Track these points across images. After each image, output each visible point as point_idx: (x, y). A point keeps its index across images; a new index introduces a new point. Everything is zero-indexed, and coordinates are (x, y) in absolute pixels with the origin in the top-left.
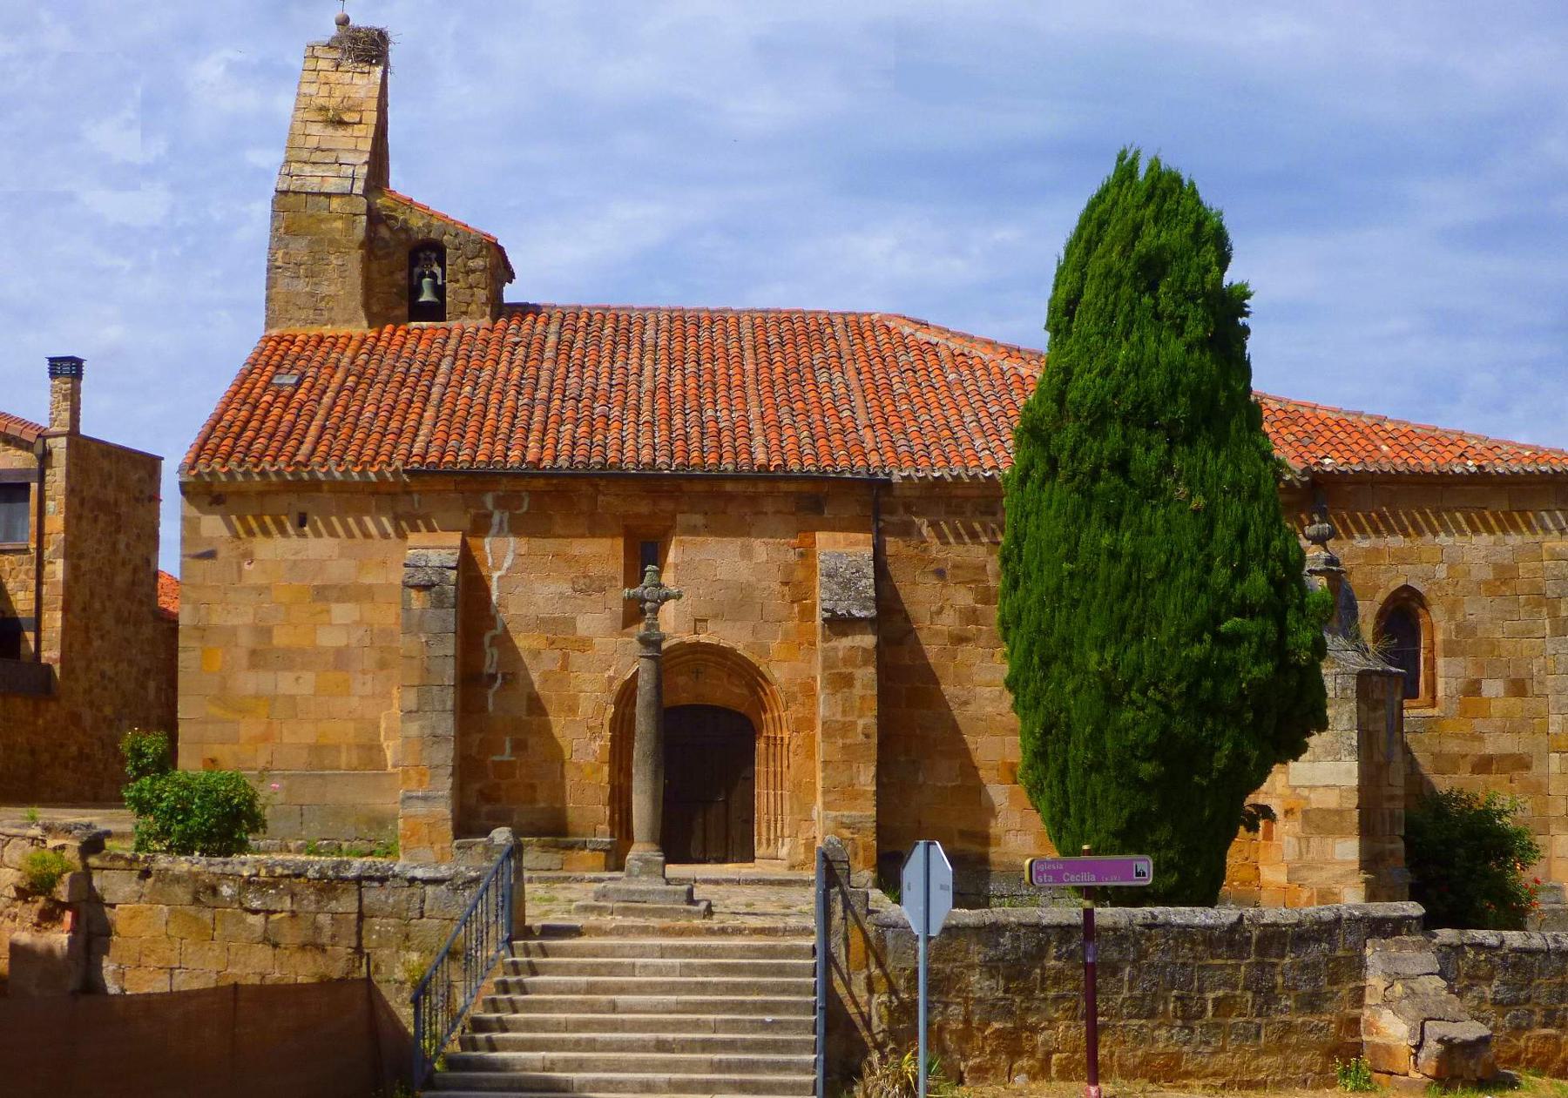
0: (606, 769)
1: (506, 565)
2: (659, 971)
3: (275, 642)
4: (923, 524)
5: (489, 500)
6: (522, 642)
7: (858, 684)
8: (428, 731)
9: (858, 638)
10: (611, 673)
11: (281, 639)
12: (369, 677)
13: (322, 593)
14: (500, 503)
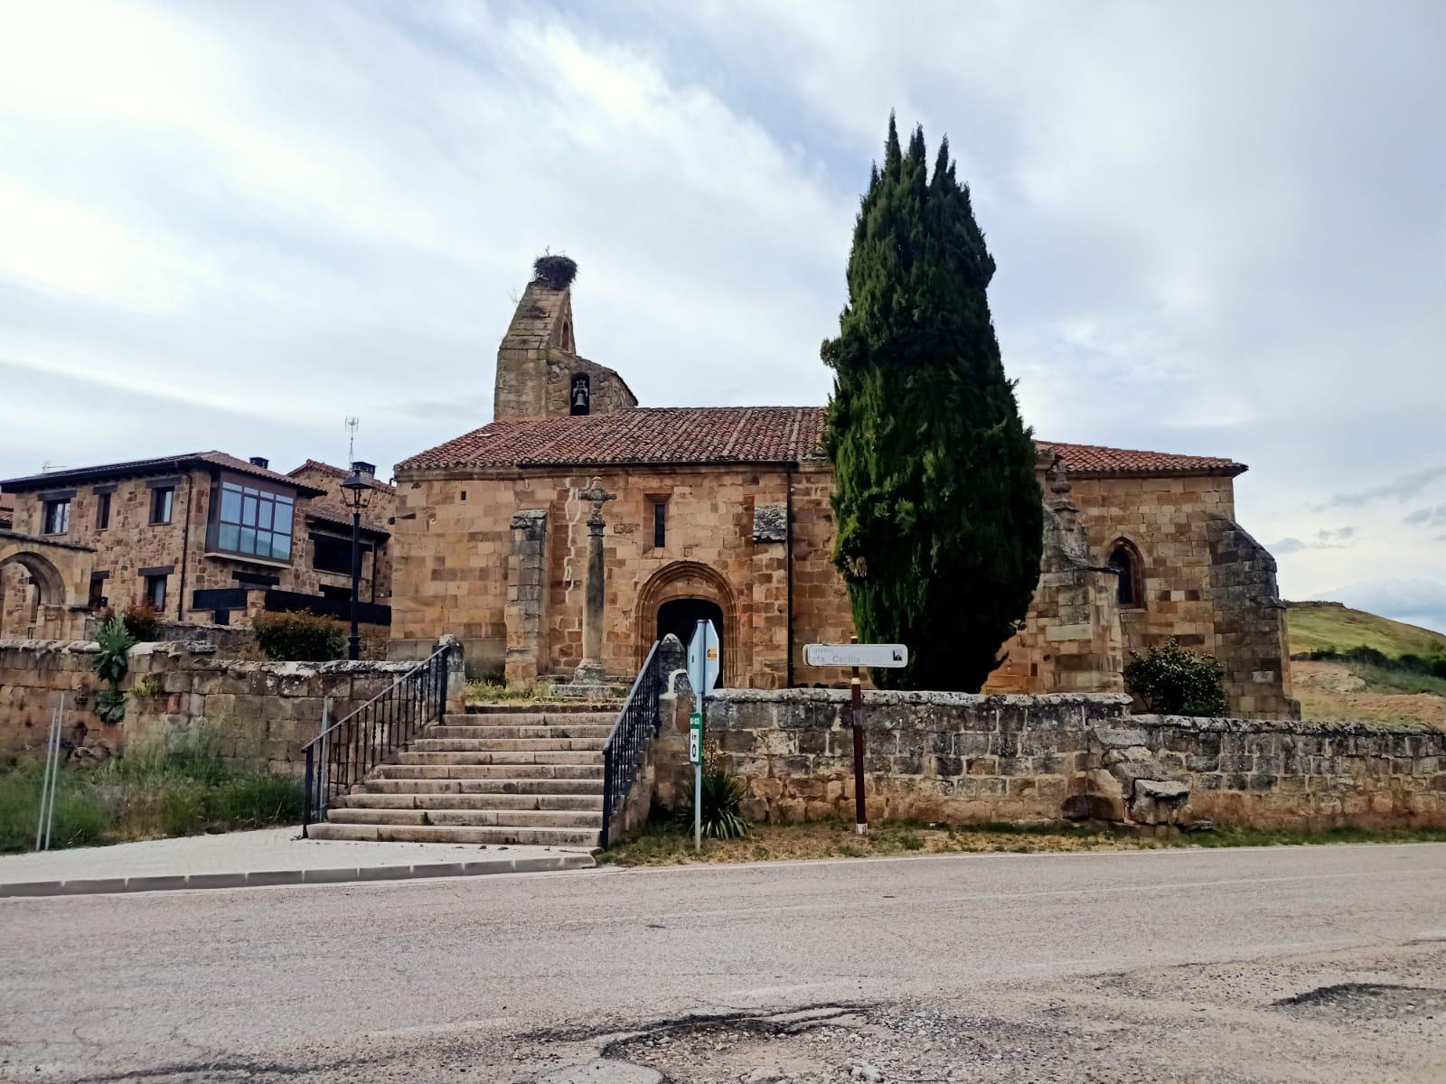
7: (774, 580)
8: (522, 612)
11: (449, 564)
13: (473, 537)
14: (573, 484)
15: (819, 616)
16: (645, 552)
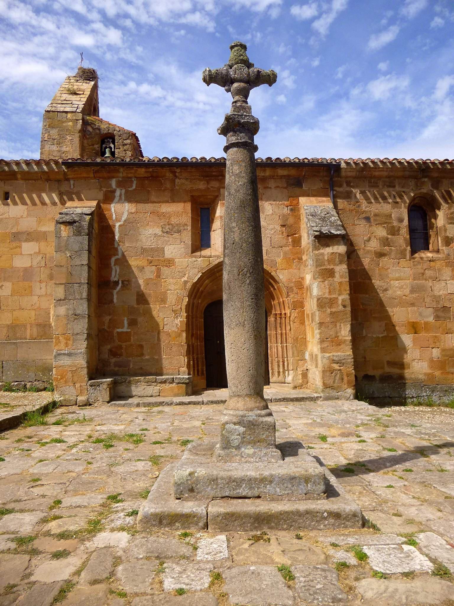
0: (184, 335)
1: (123, 219)
4: (357, 192)
5: (113, 183)
6: (133, 262)
7: (337, 275)
8: (71, 312)
12: (43, 285)
13: (17, 237)
14: (120, 184)
15: (365, 310)
16: (193, 252)
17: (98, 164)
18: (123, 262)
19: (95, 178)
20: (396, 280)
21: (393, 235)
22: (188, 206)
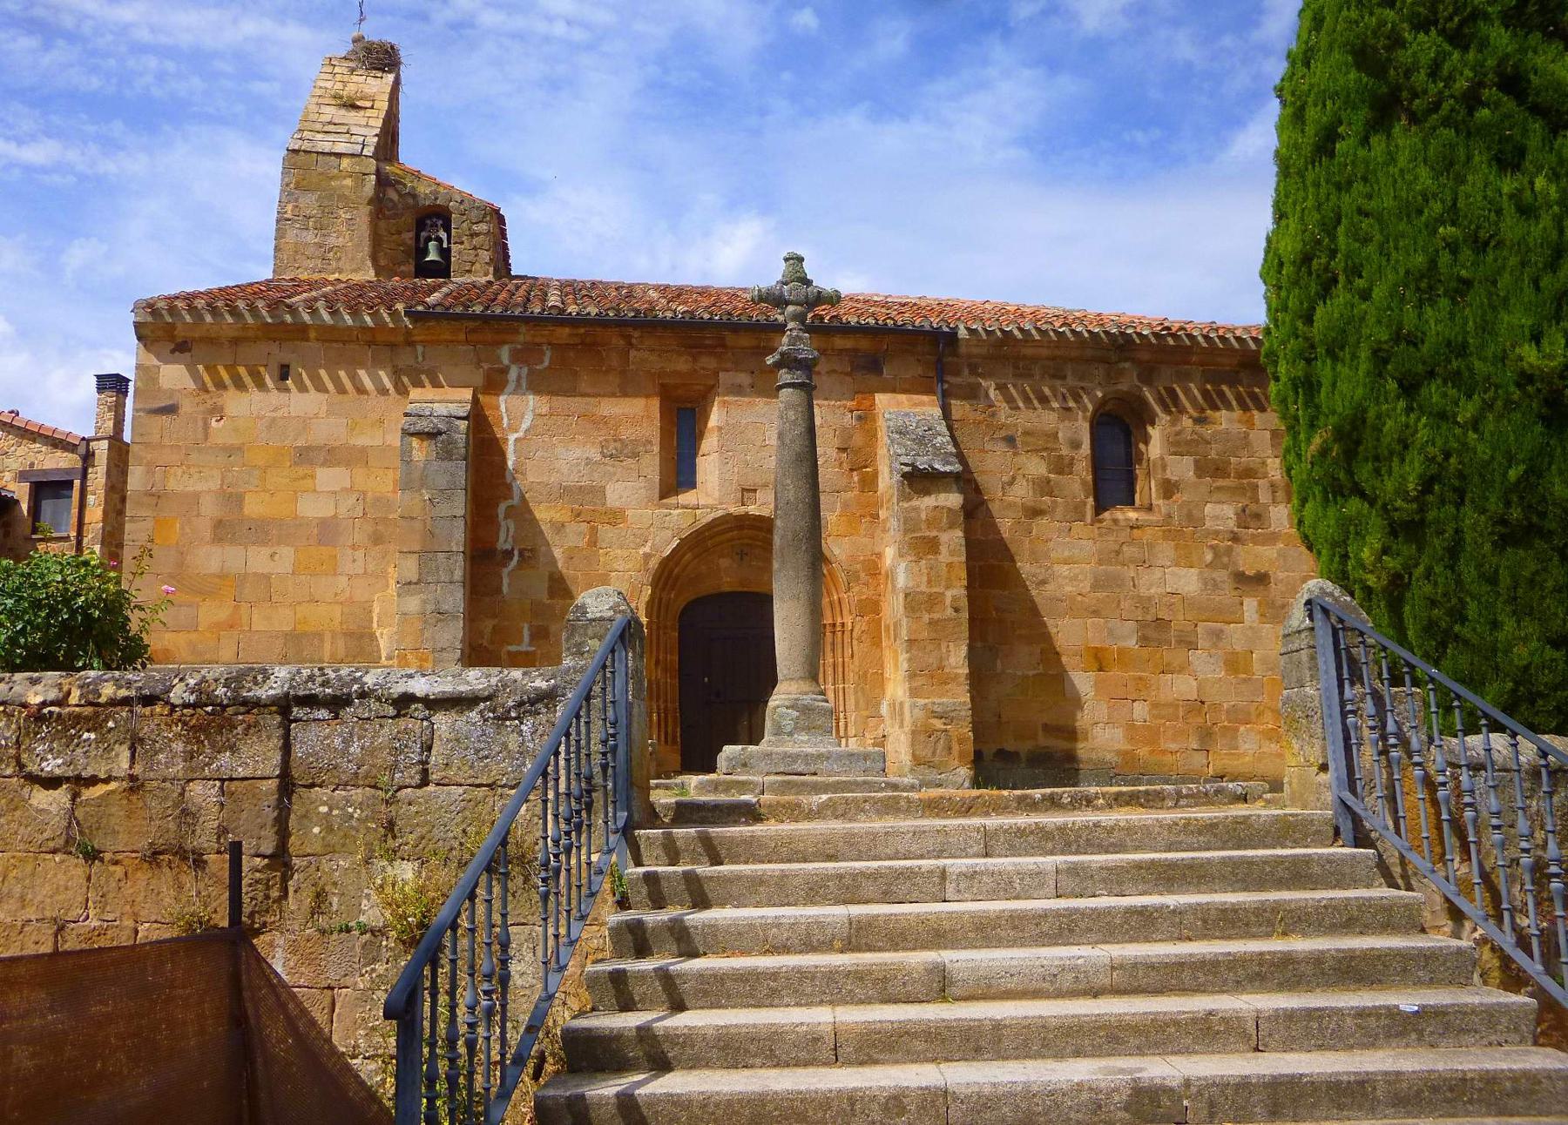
1: (524, 426)
2: (1004, 886)
3: (246, 511)
5: (505, 354)
6: (543, 514)
7: (943, 549)
8: (430, 608)
9: (942, 496)
10: (647, 549)
11: (254, 506)
12: (360, 554)
13: (306, 456)
14: (516, 357)
16: (662, 497)
17: (474, 317)
18: (523, 513)
19: (467, 342)
20: (1064, 563)
21: (1060, 472)
22: (655, 403)
